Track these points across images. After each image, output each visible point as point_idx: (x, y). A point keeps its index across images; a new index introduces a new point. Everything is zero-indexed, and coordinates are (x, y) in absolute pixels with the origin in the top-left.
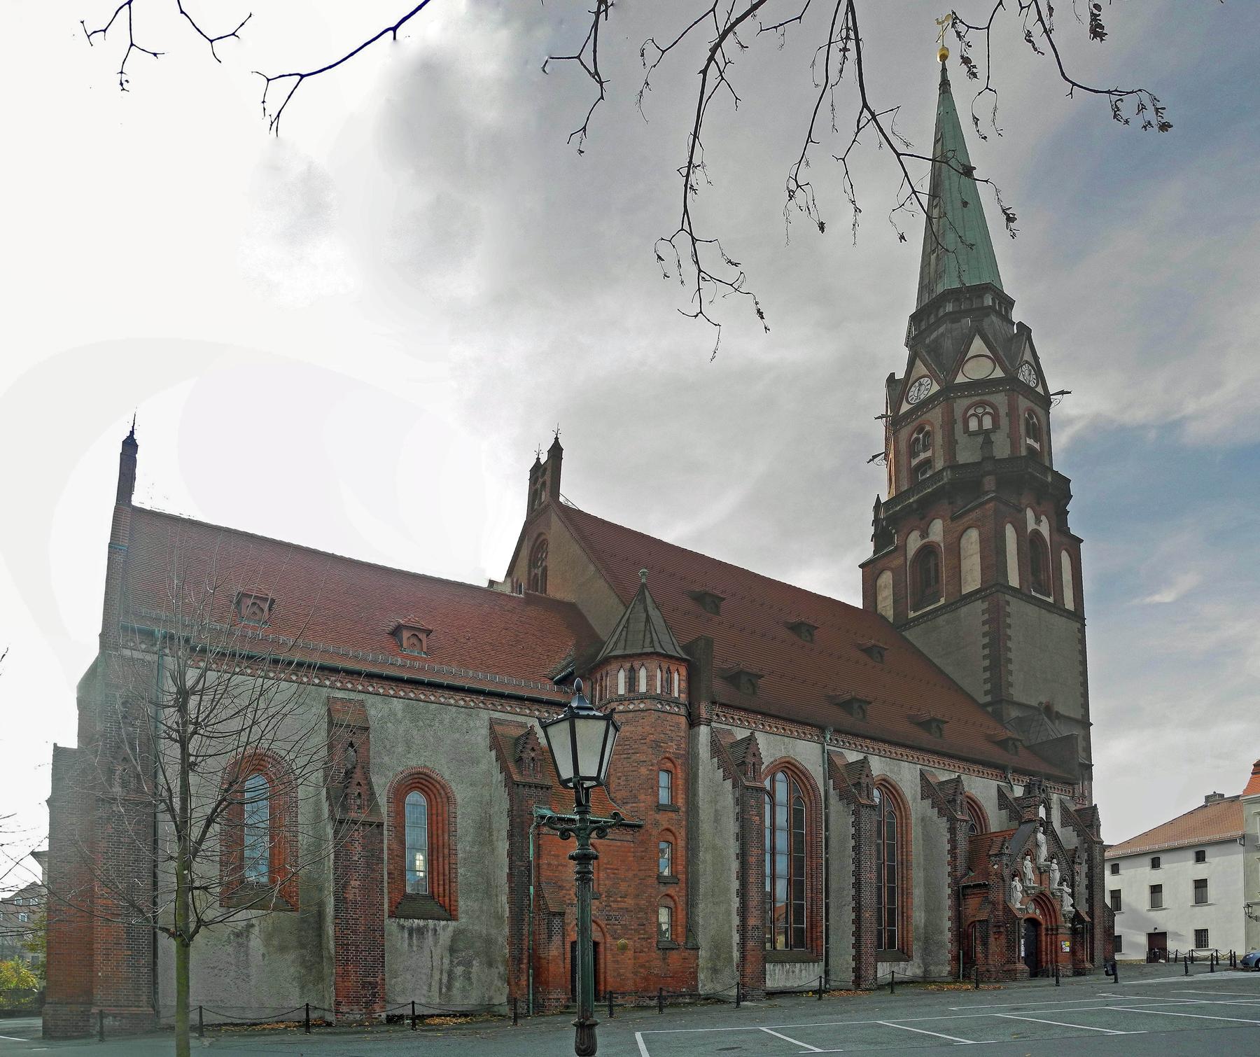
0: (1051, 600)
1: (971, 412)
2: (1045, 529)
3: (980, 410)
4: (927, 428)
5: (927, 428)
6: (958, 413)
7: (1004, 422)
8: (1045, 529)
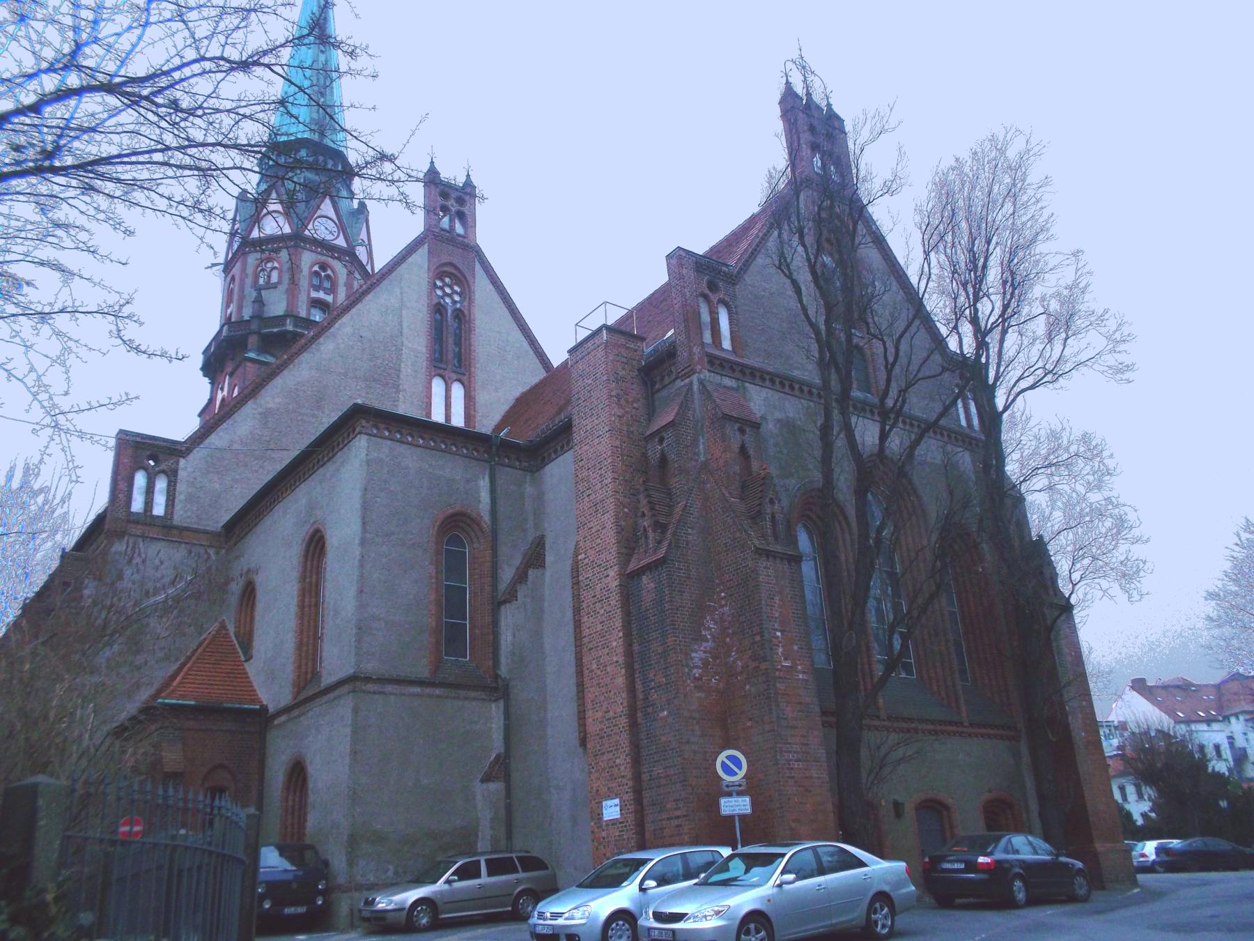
3: (269, 265)
4: (316, 268)
5: (316, 268)
6: (250, 270)
7: (286, 277)
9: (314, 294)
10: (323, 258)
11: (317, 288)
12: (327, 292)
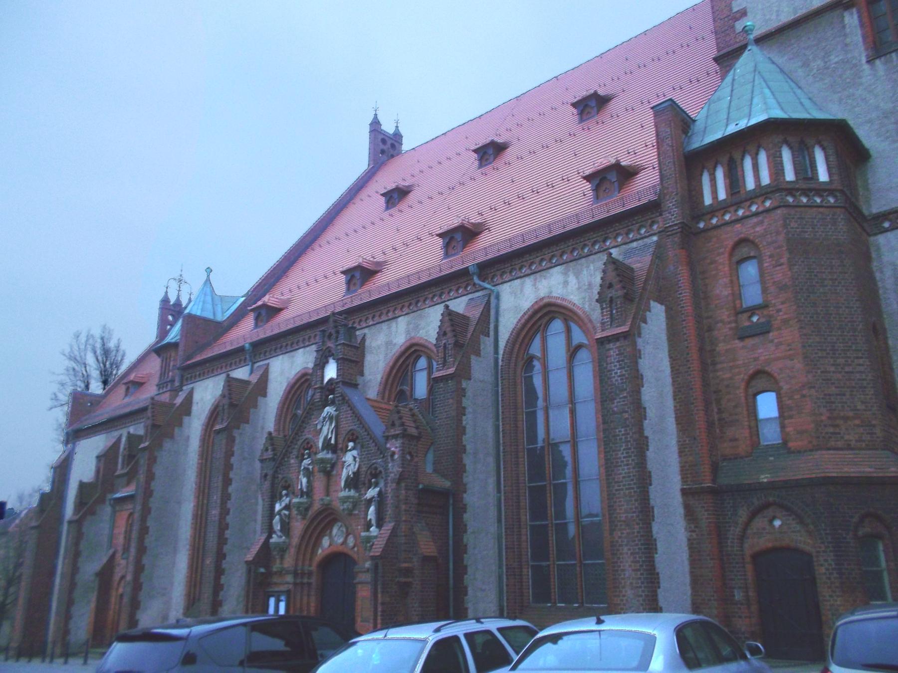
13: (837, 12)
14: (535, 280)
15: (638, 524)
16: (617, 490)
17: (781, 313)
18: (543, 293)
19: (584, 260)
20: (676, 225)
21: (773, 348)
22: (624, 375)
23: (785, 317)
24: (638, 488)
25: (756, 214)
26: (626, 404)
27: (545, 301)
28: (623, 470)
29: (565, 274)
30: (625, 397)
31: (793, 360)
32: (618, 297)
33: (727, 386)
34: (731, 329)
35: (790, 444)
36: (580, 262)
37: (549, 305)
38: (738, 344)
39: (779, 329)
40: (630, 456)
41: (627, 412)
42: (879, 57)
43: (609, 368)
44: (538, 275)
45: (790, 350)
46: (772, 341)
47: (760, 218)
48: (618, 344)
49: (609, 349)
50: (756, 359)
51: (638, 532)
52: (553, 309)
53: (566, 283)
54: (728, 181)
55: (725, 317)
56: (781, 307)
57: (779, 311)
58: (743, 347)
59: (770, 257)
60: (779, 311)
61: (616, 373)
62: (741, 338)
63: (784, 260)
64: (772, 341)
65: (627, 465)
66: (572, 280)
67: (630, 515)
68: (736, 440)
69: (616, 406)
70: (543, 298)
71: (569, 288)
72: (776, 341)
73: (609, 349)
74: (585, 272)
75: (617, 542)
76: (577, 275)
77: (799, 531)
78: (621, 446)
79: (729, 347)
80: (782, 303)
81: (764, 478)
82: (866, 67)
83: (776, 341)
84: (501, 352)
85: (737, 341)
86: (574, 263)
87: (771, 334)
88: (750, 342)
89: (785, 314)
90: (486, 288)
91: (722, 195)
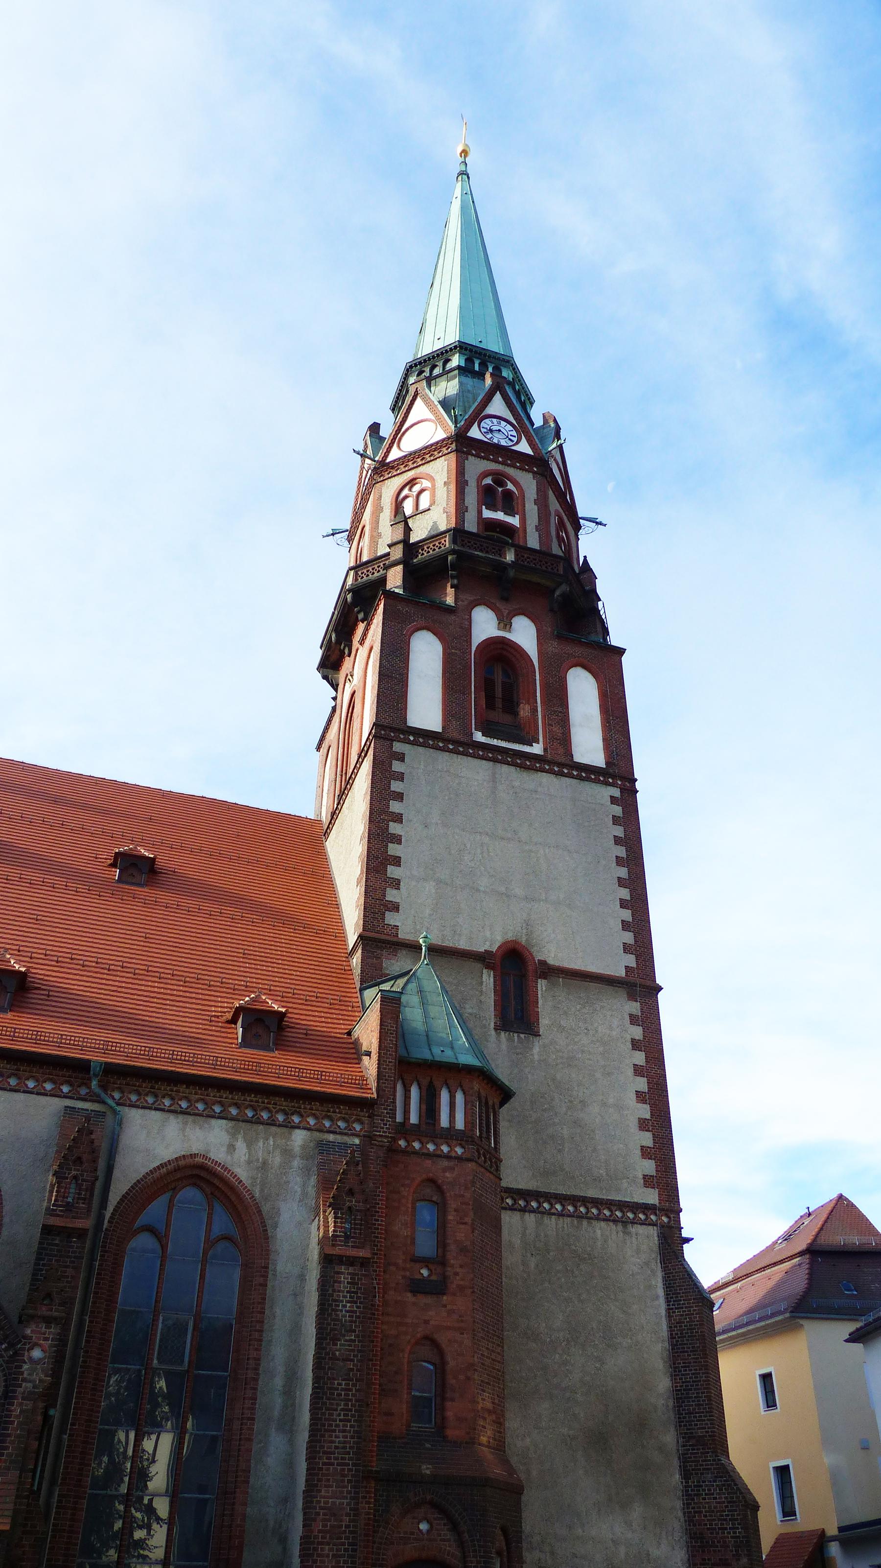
0: (537, 749)
1: (406, 492)
2: (524, 634)
4: (488, 481)
8: (524, 634)
9: (487, 514)
10: (493, 466)
11: (492, 507)
12: (510, 512)
13: (479, 965)
14: (186, 1123)
15: (348, 1515)
16: (324, 1464)
17: (458, 1278)
18: (196, 1147)
19: (261, 1127)
20: (386, 1137)
21: (445, 1314)
22: (355, 1312)
23: (462, 1283)
24: (354, 1465)
25: (448, 1157)
26: (353, 1351)
27: (199, 1160)
28: (337, 1437)
29: (233, 1135)
30: (351, 1340)
31: (463, 1334)
32: (358, 1211)
33: (391, 1345)
34: (404, 1277)
35: (450, 1433)
36: (255, 1126)
37: (202, 1167)
38: (409, 1297)
39: (454, 1294)
40: (350, 1421)
41: (352, 1360)
42: (505, 1030)
43: (335, 1297)
44: (190, 1119)
45: (462, 1321)
46: (445, 1306)
47: (452, 1164)
48: (351, 1270)
49: (338, 1273)
50: (426, 1322)
51: (347, 1526)
52: (203, 1174)
53: (231, 1148)
54: (424, 1107)
55: (400, 1262)
56: (458, 1270)
57: (456, 1274)
58: (414, 1304)
59: (455, 1210)
60: (456, 1274)
61: (345, 1306)
62: (414, 1292)
63: (468, 1220)
64: (445, 1306)
65: (344, 1431)
66: (241, 1145)
67: (338, 1501)
68: (392, 1414)
69: (340, 1348)
70: (195, 1155)
71: (236, 1156)
72: (449, 1307)
73: (338, 1273)
74: (261, 1144)
75: (316, 1537)
76: (250, 1144)
77: (449, 1540)
78: (338, 1405)
79: (399, 1298)
80: (461, 1266)
81: (427, 1470)
82: (493, 1032)
83: (449, 1307)
84: (110, 1208)
85: (409, 1295)
86: (248, 1125)
87: (445, 1298)
88: (424, 1300)
89: (462, 1280)
90: (104, 1103)
91: (414, 1119)
